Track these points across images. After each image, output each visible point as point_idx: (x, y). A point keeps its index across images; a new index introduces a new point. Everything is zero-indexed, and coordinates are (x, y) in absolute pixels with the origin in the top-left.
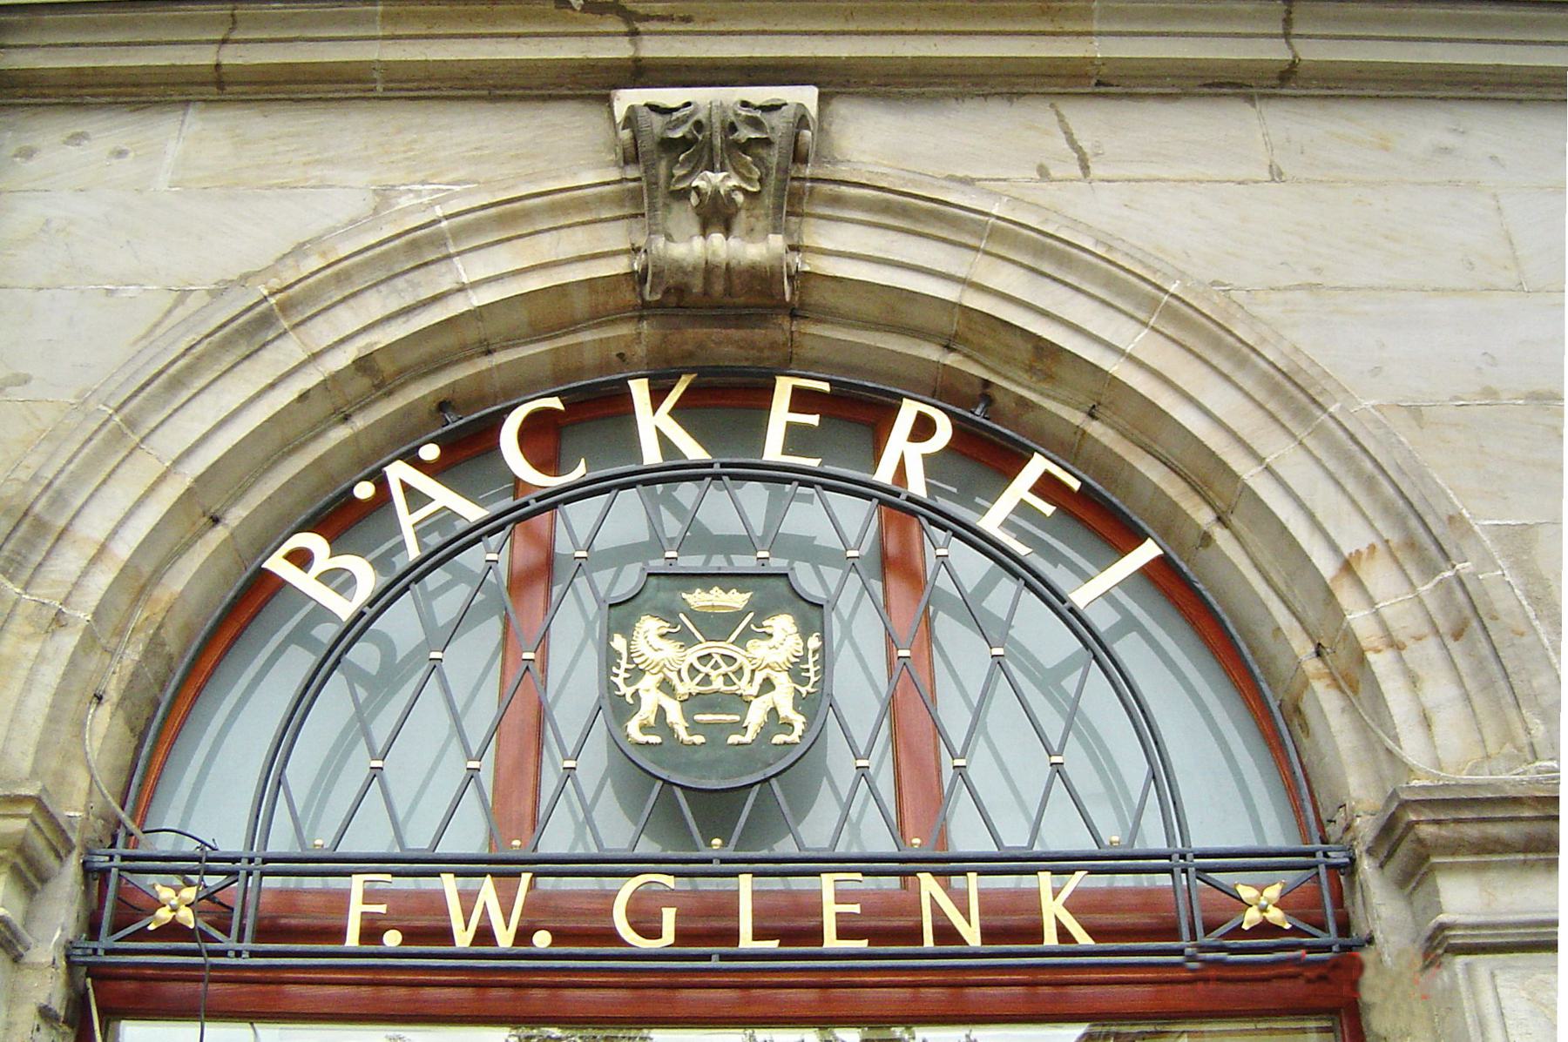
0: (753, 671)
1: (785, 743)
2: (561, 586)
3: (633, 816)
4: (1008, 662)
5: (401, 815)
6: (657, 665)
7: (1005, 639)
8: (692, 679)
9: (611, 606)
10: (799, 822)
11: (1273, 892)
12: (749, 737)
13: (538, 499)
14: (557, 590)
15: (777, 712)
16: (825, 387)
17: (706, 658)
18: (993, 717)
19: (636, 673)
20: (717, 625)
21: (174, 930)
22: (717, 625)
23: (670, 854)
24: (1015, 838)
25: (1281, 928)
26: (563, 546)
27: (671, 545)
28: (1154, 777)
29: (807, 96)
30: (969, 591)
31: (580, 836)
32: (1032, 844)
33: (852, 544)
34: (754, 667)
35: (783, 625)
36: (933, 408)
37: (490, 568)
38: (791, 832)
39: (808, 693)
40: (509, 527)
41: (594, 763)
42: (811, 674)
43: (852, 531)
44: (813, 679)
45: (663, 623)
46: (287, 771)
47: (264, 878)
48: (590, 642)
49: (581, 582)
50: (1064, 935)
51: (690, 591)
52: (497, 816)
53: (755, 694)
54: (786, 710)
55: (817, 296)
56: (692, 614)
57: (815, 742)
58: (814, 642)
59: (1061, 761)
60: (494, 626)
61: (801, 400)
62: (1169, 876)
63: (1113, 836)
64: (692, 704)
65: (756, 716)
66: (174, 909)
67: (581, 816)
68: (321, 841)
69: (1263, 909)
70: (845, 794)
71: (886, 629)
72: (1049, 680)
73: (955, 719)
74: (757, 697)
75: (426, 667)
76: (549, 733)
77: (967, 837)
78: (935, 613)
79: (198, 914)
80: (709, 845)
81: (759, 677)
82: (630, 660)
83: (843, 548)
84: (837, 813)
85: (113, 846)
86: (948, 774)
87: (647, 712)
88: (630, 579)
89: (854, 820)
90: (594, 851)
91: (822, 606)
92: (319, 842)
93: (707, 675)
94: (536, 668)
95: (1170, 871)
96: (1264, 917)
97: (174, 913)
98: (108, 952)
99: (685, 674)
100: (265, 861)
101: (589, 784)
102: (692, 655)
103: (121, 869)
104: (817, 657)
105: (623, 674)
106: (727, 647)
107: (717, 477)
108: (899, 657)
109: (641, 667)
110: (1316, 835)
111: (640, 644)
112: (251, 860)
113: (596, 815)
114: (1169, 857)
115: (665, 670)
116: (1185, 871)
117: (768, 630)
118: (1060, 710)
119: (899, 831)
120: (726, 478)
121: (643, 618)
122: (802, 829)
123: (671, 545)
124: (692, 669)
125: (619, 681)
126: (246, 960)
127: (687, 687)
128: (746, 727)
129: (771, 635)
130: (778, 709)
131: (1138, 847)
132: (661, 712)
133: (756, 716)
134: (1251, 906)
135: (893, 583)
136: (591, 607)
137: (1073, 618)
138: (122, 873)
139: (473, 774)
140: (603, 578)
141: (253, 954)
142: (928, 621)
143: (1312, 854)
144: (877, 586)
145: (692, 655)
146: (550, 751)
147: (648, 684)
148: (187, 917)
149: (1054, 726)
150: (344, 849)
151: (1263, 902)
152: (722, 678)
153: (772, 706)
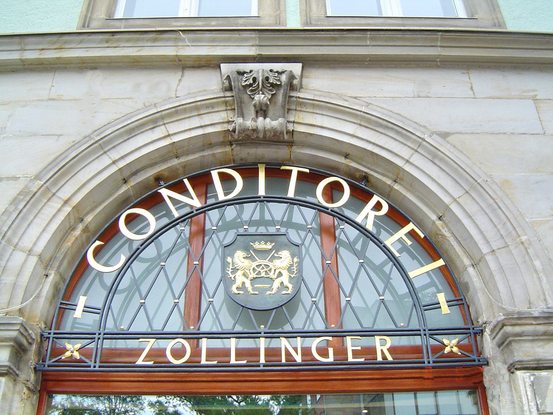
0: (275, 270)
1: (286, 294)
2: (208, 237)
3: (233, 317)
4: (365, 265)
5: (151, 316)
6: (242, 268)
7: (364, 257)
8: (254, 273)
9: (225, 247)
10: (292, 316)
11: (454, 342)
12: (273, 292)
13: (197, 210)
14: (206, 239)
15: (283, 283)
16: (308, 171)
17: (258, 266)
18: (359, 282)
19: (235, 270)
20: (263, 253)
21: (71, 359)
22: (263, 253)
23: (246, 330)
24: (367, 324)
25: (457, 354)
26: (208, 226)
27: (246, 223)
28: (415, 305)
29: (296, 68)
30: (352, 241)
31: (214, 323)
32: (373, 327)
33: (309, 223)
34: (275, 269)
35: (285, 254)
36: (341, 179)
37: (162, 268)
38: (289, 322)
39: (294, 277)
40: (187, 221)
41: (219, 299)
42: (295, 270)
43: (309, 220)
44: (295, 272)
45: (244, 253)
46: (112, 304)
47: (104, 340)
48: (217, 256)
49: (214, 236)
50: (384, 358)
51: (254, 242)
52: (186, 318)
53: (276, 278)
54: (286, 283)
55: (296, 138)
56: (255, 251)
57: (297, 292)
58: (296, 260)
59: (383, 298)
60: (183, 252)
61: (412, 234)
62: (420, 336)
63: (402, 324)
64: (253, 280)
65: (276, 284)
66: (72, 352)
67: (215, 316)
68: (124, 326)
69: (452, 347)
70: (308, 309)
71: (322, 253)
72: (378, 269)
73: (345, 282)
74: (276, 279)
75: (159, 267)
76: (203, 287)
77: (350, 324)
78: (339, 247)
79: (80, 354)
80: (260, 327)
81: (277, 272)
82: (233, 265)
83: (305, 224)
84: (305, 315)
85: (51, 329)
86: (343, 303)
87: (238, 283)
88: (230, 237)
89: (311, 317)
90: (220, 330)
91: (298, 246)
92: (122, 327)
93: (259, 272)
94: (199, 268)
95: (420, 335)
96: (452, 350)
97: (72, 353)
98: (48, 366)
99: (251, 271)
100: (104, 334)
101: (217, 306)
102: (254, 265)
103: (53, 338)
104: (297, 265)
105: (231, 270)
106: (266, 262)
107: (262, 201)
108: (327, 264)
109: (237, 268)
110: (470, 322)
111: (236, 260)
112: (100, 334)
113: (220, 316)
114: (420, 330)
115: (245, 269)
116: (425, 335)
117: (280, 256)
118: (382, 281)
119: (326, 320)
120: (265, 202)
121: (237, 251)
122: (293, 321)
123: (246, 223)
124: (254, 269)
125: (229, 273)
126: (97, 368)
127: (253, 275)
128: (273, 289)
129: (281, 258)
130: (284, 282)
131: (410, 328)
132: (243, 283)
133: (276, 284)
134: (447, 346)
135: (324, 236)
136: (218, 244)
137: (385, 249)
138: (54, 339)
139: (176, 304)
140: (221, 235)
141: (100, 367)
142: (336, 250)
143: (469, 329)
144: (318, 238)
145: (254, 265)
146: (204, 295)
147: (239, 274)
148: (77, 355)
149: (381, 286)
150: (132, 330)
151: (452, 345)
152: (264, 272)
153: (281, 281)
